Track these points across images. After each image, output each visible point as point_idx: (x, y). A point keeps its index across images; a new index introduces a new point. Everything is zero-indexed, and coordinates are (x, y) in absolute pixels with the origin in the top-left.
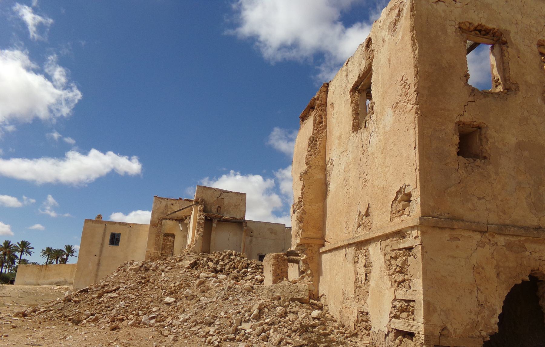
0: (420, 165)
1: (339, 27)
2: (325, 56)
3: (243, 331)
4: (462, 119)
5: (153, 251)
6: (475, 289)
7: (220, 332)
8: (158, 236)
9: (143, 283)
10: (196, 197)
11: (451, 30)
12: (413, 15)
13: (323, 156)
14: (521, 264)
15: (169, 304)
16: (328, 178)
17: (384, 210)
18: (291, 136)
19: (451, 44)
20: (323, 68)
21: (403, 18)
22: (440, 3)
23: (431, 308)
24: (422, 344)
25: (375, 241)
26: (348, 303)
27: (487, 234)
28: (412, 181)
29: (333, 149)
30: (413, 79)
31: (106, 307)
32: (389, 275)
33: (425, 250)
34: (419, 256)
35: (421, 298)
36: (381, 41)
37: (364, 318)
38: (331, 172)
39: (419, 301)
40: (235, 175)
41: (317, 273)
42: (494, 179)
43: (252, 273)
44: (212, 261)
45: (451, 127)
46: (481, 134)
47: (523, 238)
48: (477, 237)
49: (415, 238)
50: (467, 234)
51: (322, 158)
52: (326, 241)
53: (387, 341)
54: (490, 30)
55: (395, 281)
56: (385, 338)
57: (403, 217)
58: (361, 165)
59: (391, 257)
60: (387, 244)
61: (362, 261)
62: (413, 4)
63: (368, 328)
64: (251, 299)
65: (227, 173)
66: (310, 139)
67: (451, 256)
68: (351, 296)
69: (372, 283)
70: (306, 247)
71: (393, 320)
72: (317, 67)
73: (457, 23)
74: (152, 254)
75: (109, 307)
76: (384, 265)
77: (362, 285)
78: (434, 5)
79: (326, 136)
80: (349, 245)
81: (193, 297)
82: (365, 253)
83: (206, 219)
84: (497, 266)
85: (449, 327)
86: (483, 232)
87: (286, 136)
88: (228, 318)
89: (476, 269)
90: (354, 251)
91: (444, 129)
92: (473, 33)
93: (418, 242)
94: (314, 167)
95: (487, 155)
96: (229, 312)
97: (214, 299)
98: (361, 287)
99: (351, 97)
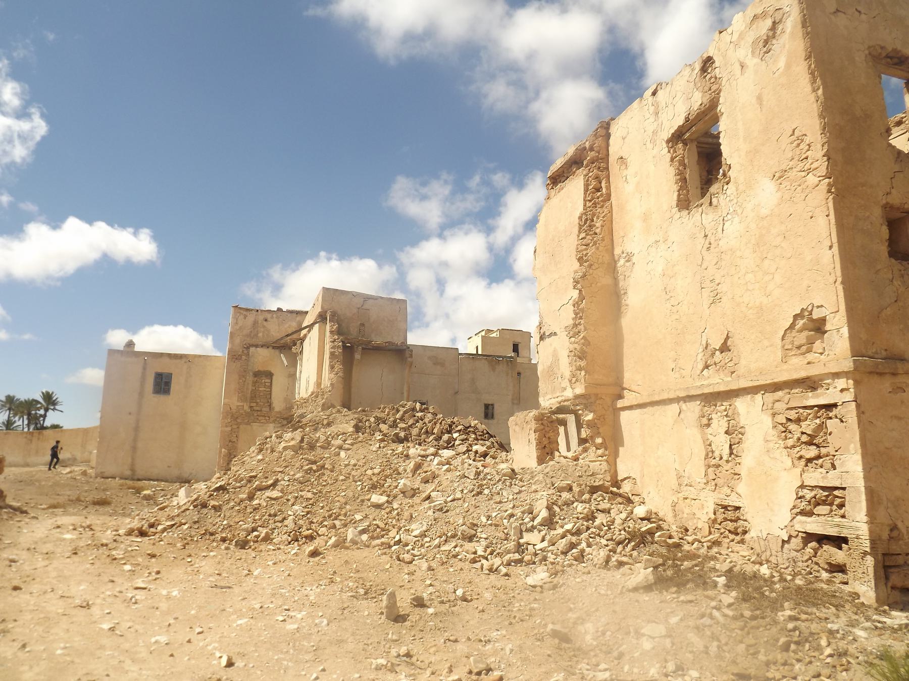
0: (843, 275)
3: (530, 547)
5: (235, 403)
8: (242, 375)
9: (315, 472)
10: (322, 308)
11: (860, 57)
12: (808, 34)
15: (378, 506)
16: (621, 284)
18: (424, 190)
21: (786, 36)
22: (839, 14)
23: (875, 499)
24: (865, 553)
25: (749, 393)
30: (819, 137)
31: (270, 515)
32: (786, 448)
33: (862, 409)
35: (861, 484)
36: (737, 67)
37: (730, 515)
38: (627, 274)
39: (856, 489)
40: (329, 259)
41: (613, 442)
44: (384, 423)
45: (877, 213)
49: (842, 391)
51: (607, 250)
53: (785, 550)
56: (782, 547)
57: (810, 357)
58: (704, 266)
59: (789, 420)
62: (804, 15)
64: (520, 492)
65: (314, 256)
66: (580, 218)
68: (699, 480)
69: (748, 459)
70: (592, 400)
71: (799, 517)
74: (234, 408)
75: (275, 515)
77: (722, 462)
78: (833, 17)
79: (611, 212)
80: (690, 398)
81: (414, 492)
82: (725, 410)
83: (344, 347)
85: (900, 525)
87: (416, 190)
90: (700, 407)
91: (868, 217)
92: (884, 61)
93: (849, 396)
94: (596, 265)
96: (494, 515)
97: (458, 495)
98: (722, 465)
99: (669, 152)
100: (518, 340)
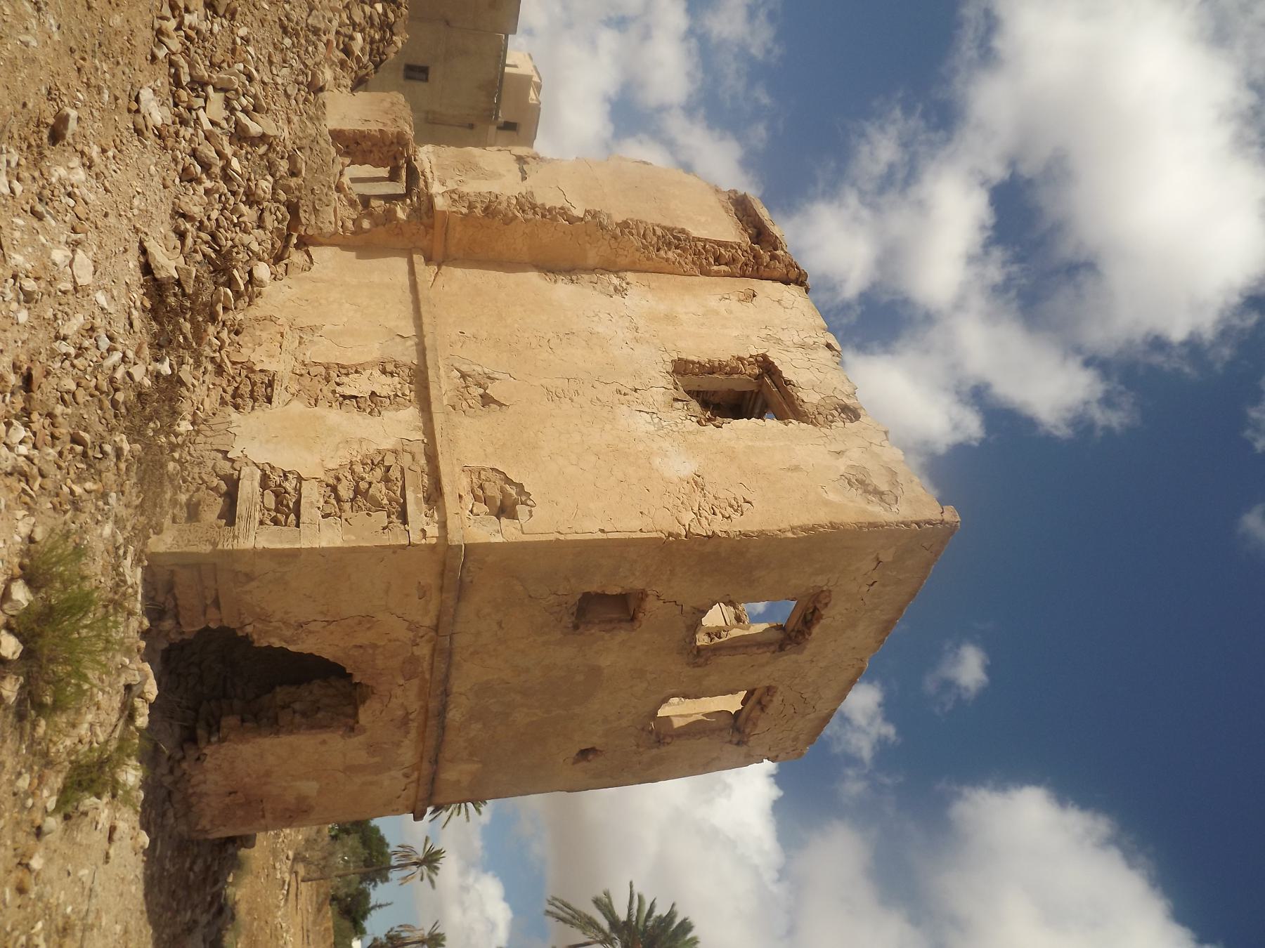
0: (568, 541)
1: (998, 172)
2: (942, 133)
3: (201, 102)
7: (192, 42)
11: (820, 581)
12: (860, 528)
13: (638, 267)
16: (586, 277)
17: (490, 450)
20: (915, 122)
24: (215, 544)
25: (425, 424)
26: (291, 342)
28: (539, 523)
29: (650, 296)
30: (737, 529)
34: (388, 539)
35: (304, 544)
37: (260, 390)
38: (598, 286)
43: (371, 17)
45: (638, 584)
46: (620, 621)
47: (427, 676)
48: (428, 621)
49: (423, 531)
52: (439, 266)
54: (809, 628)
55: (338, 479)
56: (218, 451)
57: (469, 499)
58: (597, 384)
59: (388, 469)
60: (417, 457)
61: (384, 385)
63: (239, 401)
64: (288, 96)
66: (683, 231)
68: (308, 354)
69: (335, 417)
70: (425, 220)
72: (920, 107)
76: (372, 449)
79: (685, 274)
80: (422, 351)
84: (375, 646)
85: (254, 584)
86: (436, 628)
88: (233, 51)
90: (409, 363)
93: (416, 538)
95: (581, 629)
98: (328, 383)
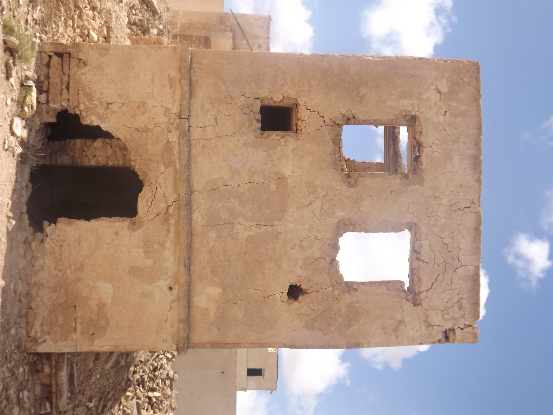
4: (302, 107)
6: (122, 101)
14: (150, 159)
19: (389, 103)
23: (103, 51)
27: (178, 121)
42: (239, 140)
45: (291, 93)
48: (175, 109)
50: (177, 97)
67: (153, 77)
73: (418, 114)
78: (434, 87)
84: (147, 130)
85: (87, 68)
89: (142, 106)
91: (287, 84)
100: (266, 374)
